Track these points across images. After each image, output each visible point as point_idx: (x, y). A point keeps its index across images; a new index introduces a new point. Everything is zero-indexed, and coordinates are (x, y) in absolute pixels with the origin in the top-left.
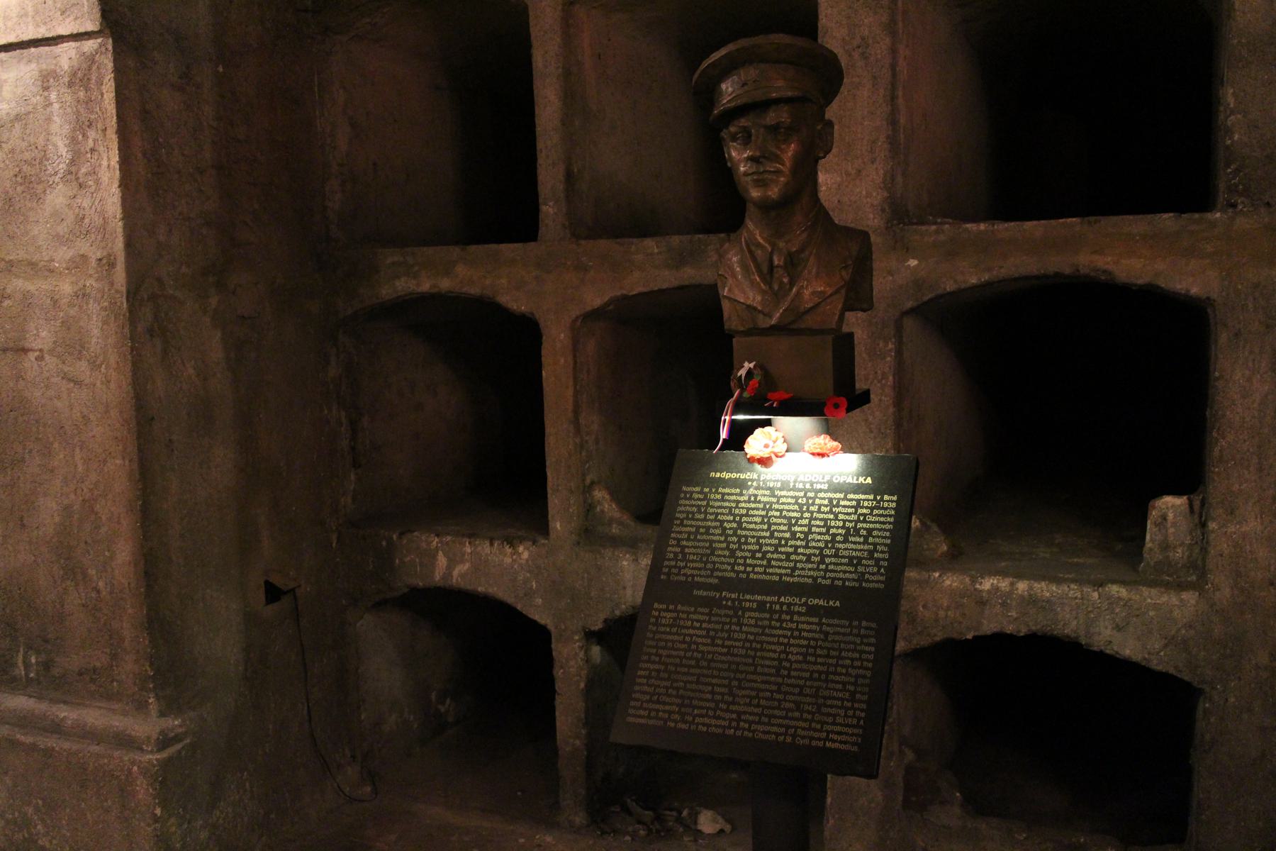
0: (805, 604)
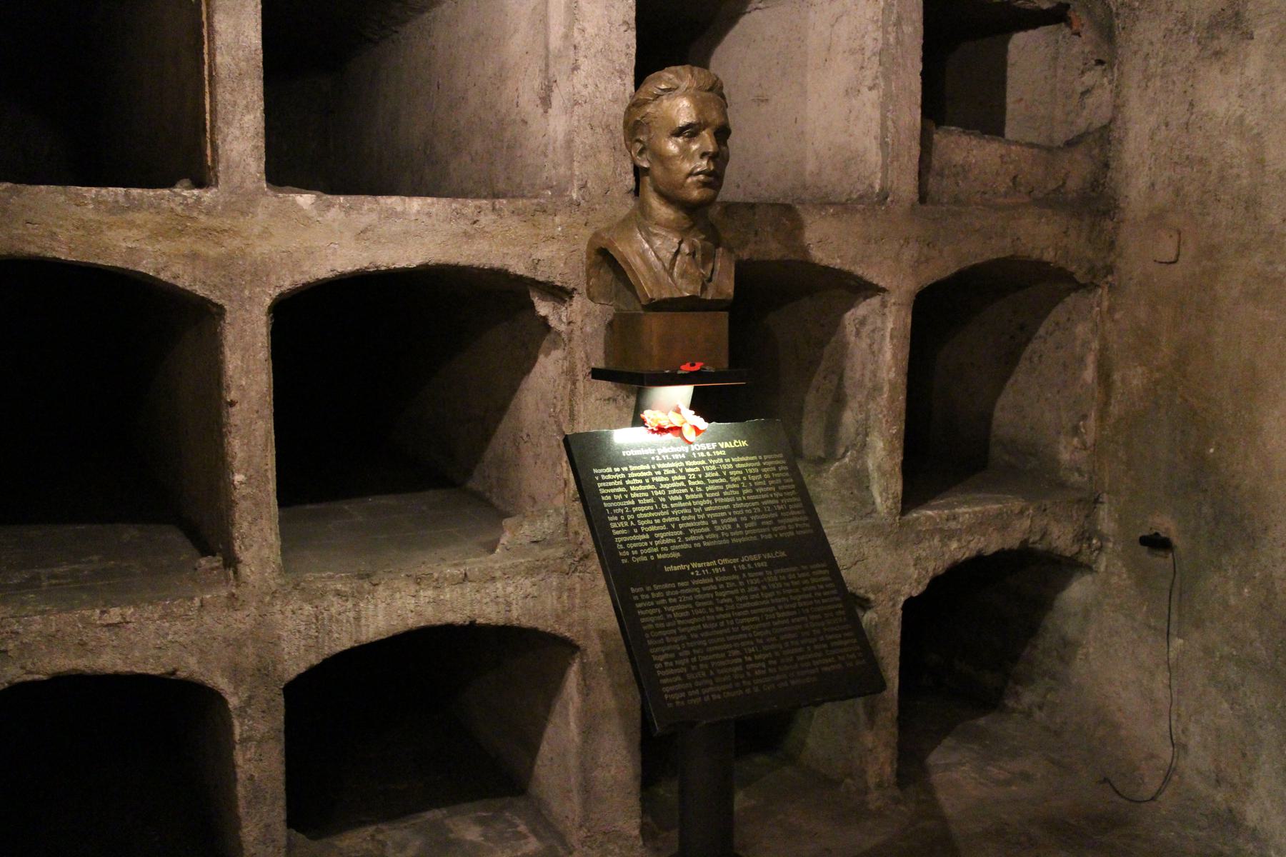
0: (762, 560)
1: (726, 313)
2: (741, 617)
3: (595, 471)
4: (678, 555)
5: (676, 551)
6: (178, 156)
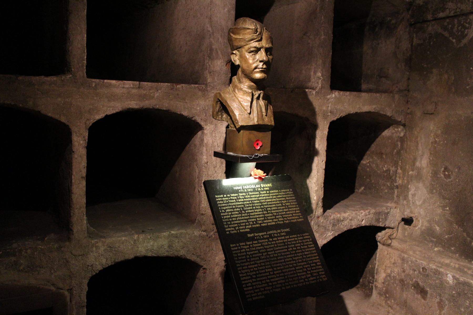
1: (270, 132)
2: (273, 261)
3: (216, 196)
4: (249, 230)
5: (248, 228)
6: (58, 64)
